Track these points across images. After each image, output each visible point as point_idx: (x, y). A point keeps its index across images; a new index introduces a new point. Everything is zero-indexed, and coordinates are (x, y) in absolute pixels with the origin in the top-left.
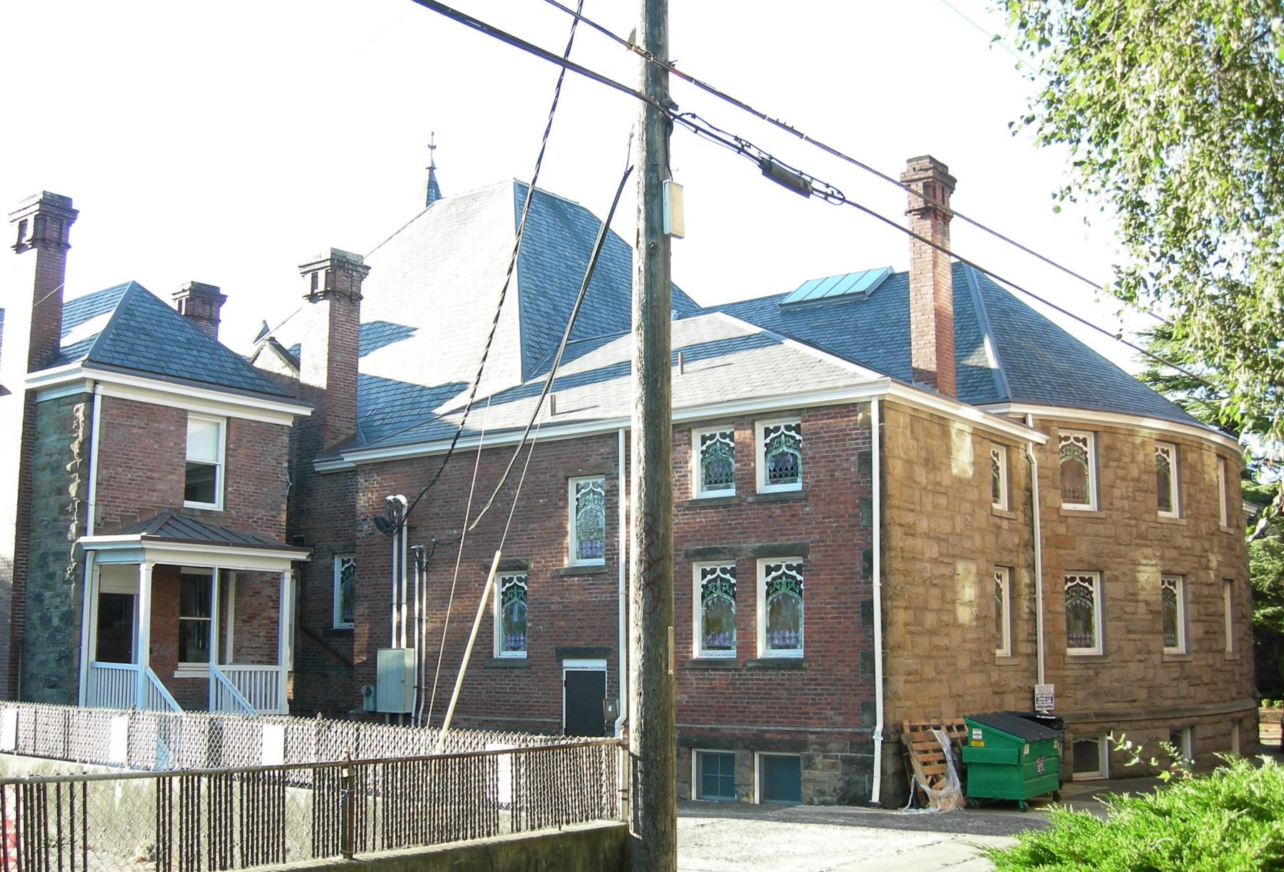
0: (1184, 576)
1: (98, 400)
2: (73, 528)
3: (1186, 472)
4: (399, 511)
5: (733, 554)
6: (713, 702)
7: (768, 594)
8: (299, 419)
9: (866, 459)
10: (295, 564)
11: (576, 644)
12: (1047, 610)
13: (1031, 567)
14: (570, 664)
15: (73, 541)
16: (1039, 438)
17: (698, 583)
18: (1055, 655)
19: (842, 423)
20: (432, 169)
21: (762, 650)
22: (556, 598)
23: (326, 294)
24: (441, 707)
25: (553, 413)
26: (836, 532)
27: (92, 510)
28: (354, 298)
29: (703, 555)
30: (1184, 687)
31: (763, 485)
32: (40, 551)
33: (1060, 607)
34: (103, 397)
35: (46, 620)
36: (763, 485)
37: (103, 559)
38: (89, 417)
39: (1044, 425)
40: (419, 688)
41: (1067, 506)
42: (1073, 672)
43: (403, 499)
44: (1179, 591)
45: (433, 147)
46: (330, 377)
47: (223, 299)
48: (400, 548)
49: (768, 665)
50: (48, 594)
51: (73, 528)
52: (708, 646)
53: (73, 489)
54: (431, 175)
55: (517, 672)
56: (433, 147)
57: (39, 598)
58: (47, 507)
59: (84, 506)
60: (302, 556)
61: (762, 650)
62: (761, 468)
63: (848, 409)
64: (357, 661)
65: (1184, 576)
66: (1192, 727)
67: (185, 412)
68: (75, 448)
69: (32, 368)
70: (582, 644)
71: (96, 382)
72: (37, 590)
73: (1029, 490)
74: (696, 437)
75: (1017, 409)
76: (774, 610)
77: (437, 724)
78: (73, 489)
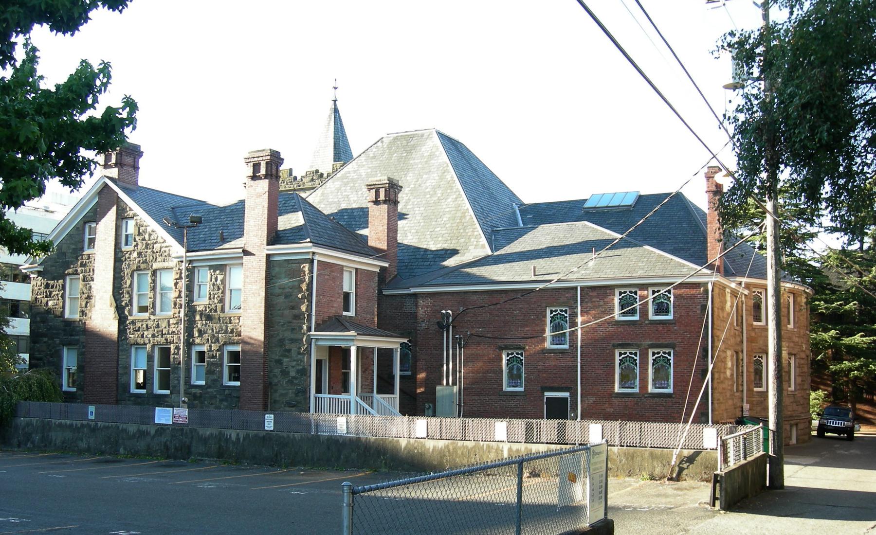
0: (795, 355)
1: (315, 263)
2: (305, 327)
3: (797, 307)
4: (448, 318)
5: (638, 346)
6: (627, 412)
7: (653, 364)
8: (383, 269)
9: (704, 307)
10: (401, 344)
11: (552, 385)
12: (747, 371)
13: (742, 352)
14: (548, 394)
15: (304, 334)
16: (746, 292)
17: (617, 359)
18: (750, 390)
19: (693, 292)
20: (335, 101)
21: (651, 389)
22: (540, 363)
23: (385, 202)
24: (688, 415)
25: (535, 275)
26: (689, 338)
27: (314, 318)
28: (396, 203)
29: (622, 346)
30: (795, 407)
31: (652, 316)
32: (278, 338)
33: (752, 370)
34: (318, 261)
35: (285, 373)
36: (652, 316)
37: (321, 343)
38: (311, 271)
39: (748, 286)
40: (460, 405)
41: (755, 323)
42: (756, 399)
43: (450, 312)
44: (792, 362)
45: (336, 88)
46: (388, 245)
47: (140, 154)
48: (448, 338)
49: (654, 396)
50: (285, 360)
51: (305, 327)
52: (622, 386)
53: (303, 308)
54: (335, 104)
55: (518, 398)
56: (336, 88)
57: (279, 362)
58: (282, 316)
59: (310, 316)
60: (405, 341)
61: (651, 389)
62: (651, 309)
63: (697, 285)
64: (418, 391)
65: (795, 355)
66: (797, 425)
67: (342, 266)
68: (304, 287)
69: (269, 243)
70: (556, 385)
71: (314, 253)
72: (277, 358)
73: (742, 317)
74: (617, 292)
75: (739, 279)
76: (657, 371)
77: (686, 421)
78: (303, 308)
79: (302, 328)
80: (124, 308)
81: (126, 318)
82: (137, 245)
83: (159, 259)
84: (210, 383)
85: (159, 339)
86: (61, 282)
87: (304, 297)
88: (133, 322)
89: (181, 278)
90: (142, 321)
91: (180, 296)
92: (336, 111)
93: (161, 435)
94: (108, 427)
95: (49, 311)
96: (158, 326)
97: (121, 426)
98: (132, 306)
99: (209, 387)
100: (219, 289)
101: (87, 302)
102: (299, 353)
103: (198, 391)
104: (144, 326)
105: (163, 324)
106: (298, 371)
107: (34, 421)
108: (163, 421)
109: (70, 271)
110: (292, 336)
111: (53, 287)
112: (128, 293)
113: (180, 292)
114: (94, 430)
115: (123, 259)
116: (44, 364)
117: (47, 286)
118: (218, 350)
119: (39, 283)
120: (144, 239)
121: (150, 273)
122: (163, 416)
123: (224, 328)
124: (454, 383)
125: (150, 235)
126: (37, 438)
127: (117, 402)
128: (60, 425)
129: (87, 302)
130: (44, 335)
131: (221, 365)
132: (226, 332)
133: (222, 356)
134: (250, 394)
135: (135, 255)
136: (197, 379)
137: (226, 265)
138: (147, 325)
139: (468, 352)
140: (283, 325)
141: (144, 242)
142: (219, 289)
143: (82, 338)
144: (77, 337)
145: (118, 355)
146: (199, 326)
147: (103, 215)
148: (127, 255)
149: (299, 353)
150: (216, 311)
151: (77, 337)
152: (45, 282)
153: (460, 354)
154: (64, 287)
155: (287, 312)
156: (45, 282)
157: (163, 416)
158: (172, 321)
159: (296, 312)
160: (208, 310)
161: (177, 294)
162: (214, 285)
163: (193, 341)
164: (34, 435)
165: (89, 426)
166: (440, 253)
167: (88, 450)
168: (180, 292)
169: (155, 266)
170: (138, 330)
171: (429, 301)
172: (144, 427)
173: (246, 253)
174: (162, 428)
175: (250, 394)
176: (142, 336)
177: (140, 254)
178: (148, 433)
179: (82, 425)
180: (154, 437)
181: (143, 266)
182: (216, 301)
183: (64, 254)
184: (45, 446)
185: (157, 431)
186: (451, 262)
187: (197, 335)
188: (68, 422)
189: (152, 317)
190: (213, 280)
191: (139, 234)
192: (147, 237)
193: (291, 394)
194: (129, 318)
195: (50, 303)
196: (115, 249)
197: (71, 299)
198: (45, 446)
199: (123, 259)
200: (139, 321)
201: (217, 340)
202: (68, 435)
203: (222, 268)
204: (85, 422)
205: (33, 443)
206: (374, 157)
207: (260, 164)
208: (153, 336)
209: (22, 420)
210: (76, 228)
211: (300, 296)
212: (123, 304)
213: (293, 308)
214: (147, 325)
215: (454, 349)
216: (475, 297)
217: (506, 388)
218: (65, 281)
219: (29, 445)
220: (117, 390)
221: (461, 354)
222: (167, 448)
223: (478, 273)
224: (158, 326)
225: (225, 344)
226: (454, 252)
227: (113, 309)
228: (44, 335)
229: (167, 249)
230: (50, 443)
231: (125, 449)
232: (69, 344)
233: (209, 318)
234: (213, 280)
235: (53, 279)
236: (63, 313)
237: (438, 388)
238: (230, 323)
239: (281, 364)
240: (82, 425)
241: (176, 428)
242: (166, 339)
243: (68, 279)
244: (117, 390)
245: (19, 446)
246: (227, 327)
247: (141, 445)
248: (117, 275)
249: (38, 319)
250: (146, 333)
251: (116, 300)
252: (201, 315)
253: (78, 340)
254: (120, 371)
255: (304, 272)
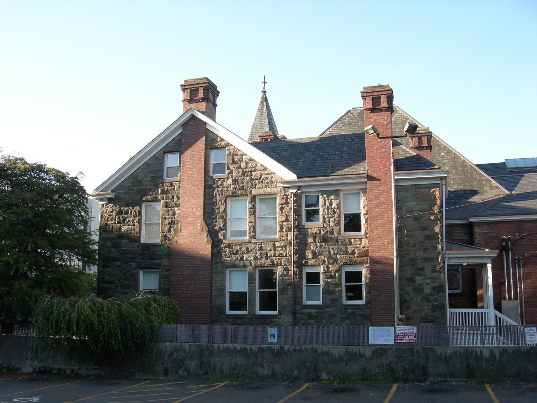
56: (265, 83)
72: (408, 276)
79: (436, 248)
80: (217, 232)
81: (221, 242)
82: (231, 172)
83: (259, 185)
84: (328, 302)
85: (263, 261)
86: (137, 208)
87: (436, 219)
88: (229, 246)
89: (287, 203)
90: (241, 244)
91: (287, 220)
92: (265, 99)
93: (381, 356)
94: (300, 351)
95: (122, 236)
96: (261, 249)
97: (320, 348)
98: (226, 230)
99: (328, 306)
100: (334, 213)
101: (170, 228)
102: (434, 271)
103: (313, 311)
104: (244, 249)
105: (268, 247)
106: (434, 288)
107: (187, 346)
108: (381, 341)
109: (149, 198)
110: (425, 255)
111: (127, 213)
112: (222, 217)
113: (287, 216)
114: (279, 354)
115: (215, 186)
116: (117, 287)
117: (120, 212)
118: (337, 271)
119: (109, 210)
120: (240, 167)
121: (248, 199)
122: (380, 336)
123: (344, 249)
124: (516, 298)
125: (247, 163)
126: (193, 365)
127: (212, 323)
128: (227, 350)
129: (170, 228)
130: (114, 259)
131: (341, 285)
132: (346, 253)
133: (340, 276)
134: (382, 312)
135: (230, 181)
136: (308, 300)
137: (339, 190)
138: (247, 249)
139: (526, 271)
140: (414, 246)
141: (240, 170)
142: (334, 213)
143: (165, 262)
144: (159, 261)
145: (212, 278)
146: (312, 248)
147: (190, 145)
148: (219, 183)
149: (434, 271)
150: (332, 233)
151: (159, 261)
152: (117, 208)
153: (520, 273)
154: (140, 213)
155: (417, 233)
156: (117, 208)
157: (380, 336)
158: (277, 244)
159: (427, 233)
160: (322, 233)
161: (284, 218)
162: (328, 209)
163: (306, 262)
164: (187, 362)
165: (271, 350)
166: (459, 193)
167: (274, 376)
168: (287, 216)
169: (254, 192)
170: (237, 253)
171: (485, 229)
172: (355, 349)
173: (370, 178)
174: (381, 350)
175: (382, 312)
176: (242, 259)
177: (235, 181)
178: (362, 356)
179: (260, 349)
180: (370, 359)
181: (239, 192)
182: (332, 224)
183: (141, 182)
184: (207, 373)
185: (374, 353)
186: (475, 199)
187: (310, 256)
188: (239, 346)
189: (253, 241)
190: (327, 204)
191: (234, 162)
192: (243, 165)
193: (427, 310)
194: (224, 241)
195: (124, 229)
196: (205, 176)
197: (146, 224)
198: (207, 373)
199: (215, 186)
200: (236, 244)
201: (336, 261)
202: (239, 360)
203: (336, 193)
204: (265, 346)
205: (187, 370)
206: (350, 124)
207: (379, 98)
208: (256, 258)
209: (168, 345)
210: (155, 157)
211: (432, 218)
212: (217, 228)
213: (424, 229)
214: (247, 249)
215: (514, 268)
216: (529, 225)
217: (229, 312)
218: (141, 207)
219: (181, 372)
220: (211, 311)
221: (520, 272)
222: (392, 371)
223: (523, 206)
224: (261, 249)
225: (346, 264)
226: (474, 193)
227: (205, 234)
228: (114, 259)
229: (269, 176)
230: (214, 370)
231: (328, 373)
232: (148, 268)
233: (325, 240)
234: (327, 204)
235: (127, 205)
236: (139, 238)
237: (503, 302)
238: (351, 244)
239: (414, 282)
240: (260, 349)
241: (401, 349)
242: (272, 262)
243: (144, 205)
244: (211, 311)
245: (166, 373)
246: (347, 248)
247: (354, 368)
248: (207, 201)
249: (109, 244)
250: (245, 256)
251: (207, 225)
252: (315, 238)
253: (160, 264)
254: (214, 293)
255: (435, 195)
